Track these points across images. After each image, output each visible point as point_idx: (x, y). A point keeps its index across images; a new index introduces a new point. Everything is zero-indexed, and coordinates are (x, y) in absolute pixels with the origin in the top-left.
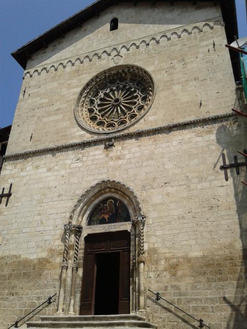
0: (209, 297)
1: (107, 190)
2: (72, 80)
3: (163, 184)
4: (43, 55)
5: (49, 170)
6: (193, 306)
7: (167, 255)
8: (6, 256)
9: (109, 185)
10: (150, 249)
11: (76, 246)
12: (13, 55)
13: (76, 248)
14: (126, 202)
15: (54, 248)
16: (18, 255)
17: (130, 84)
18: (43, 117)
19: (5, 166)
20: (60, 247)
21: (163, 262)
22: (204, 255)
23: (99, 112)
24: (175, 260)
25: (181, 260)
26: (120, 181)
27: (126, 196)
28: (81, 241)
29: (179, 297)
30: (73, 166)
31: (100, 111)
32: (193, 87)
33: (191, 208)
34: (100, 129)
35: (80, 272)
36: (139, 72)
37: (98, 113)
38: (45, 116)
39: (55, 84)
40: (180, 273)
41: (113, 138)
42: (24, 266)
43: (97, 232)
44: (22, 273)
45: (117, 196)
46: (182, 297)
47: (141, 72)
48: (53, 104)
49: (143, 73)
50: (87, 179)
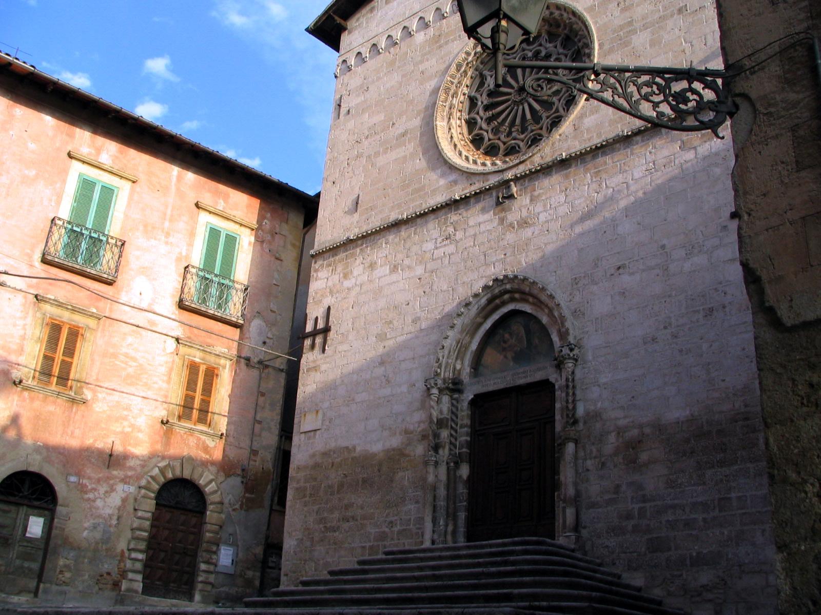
0: (700, 500)
1: (506, 297)
2: (427, 60)
3: (613, 271)
4: (369, 15)
5: (394, 269)
6: (668, 521)
7: (622, 423)
8: (330, 451)
9: (508, 286)
10: (587, 414)
11: (452, 420)
12: (307, 30)
13: (453, 425)
14: (545, 320)
15: (412, 428)
16: (350, 447)
17: (548, 45)
18: (377, 154)
19: (316, 271)
20: (422, 424)
21: (612, 438)
22: (692, 415)
23: (488, 124)
24: (635, 432)
25: (647, 430)
26: (528, 275)
27: (543, 307)
28: (462, 410)
29: (642, 505)
30: (439, 253)
31: (489, 120)
32: (676, 30)
33: (670, 318)
34: (488, 163)
35: (464, 471)
36: (562, 15)
37: (484, 126)
38: (379, 152)
39: (396, 77)
40: (644, 457)
41: (511, 180)
42: (363, 467)
43: (491, 388)
44: (361, 480)
45: (527, 308)
46: (648, 505)
47: (565, 15)
48: (393, 124)
49: (571, 16)
50: (465, 279)
